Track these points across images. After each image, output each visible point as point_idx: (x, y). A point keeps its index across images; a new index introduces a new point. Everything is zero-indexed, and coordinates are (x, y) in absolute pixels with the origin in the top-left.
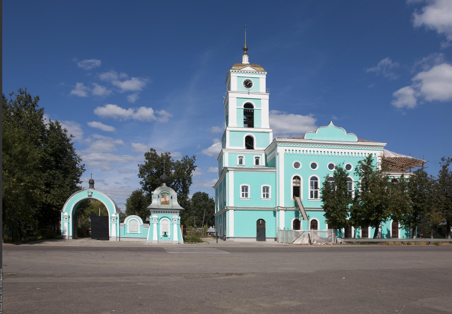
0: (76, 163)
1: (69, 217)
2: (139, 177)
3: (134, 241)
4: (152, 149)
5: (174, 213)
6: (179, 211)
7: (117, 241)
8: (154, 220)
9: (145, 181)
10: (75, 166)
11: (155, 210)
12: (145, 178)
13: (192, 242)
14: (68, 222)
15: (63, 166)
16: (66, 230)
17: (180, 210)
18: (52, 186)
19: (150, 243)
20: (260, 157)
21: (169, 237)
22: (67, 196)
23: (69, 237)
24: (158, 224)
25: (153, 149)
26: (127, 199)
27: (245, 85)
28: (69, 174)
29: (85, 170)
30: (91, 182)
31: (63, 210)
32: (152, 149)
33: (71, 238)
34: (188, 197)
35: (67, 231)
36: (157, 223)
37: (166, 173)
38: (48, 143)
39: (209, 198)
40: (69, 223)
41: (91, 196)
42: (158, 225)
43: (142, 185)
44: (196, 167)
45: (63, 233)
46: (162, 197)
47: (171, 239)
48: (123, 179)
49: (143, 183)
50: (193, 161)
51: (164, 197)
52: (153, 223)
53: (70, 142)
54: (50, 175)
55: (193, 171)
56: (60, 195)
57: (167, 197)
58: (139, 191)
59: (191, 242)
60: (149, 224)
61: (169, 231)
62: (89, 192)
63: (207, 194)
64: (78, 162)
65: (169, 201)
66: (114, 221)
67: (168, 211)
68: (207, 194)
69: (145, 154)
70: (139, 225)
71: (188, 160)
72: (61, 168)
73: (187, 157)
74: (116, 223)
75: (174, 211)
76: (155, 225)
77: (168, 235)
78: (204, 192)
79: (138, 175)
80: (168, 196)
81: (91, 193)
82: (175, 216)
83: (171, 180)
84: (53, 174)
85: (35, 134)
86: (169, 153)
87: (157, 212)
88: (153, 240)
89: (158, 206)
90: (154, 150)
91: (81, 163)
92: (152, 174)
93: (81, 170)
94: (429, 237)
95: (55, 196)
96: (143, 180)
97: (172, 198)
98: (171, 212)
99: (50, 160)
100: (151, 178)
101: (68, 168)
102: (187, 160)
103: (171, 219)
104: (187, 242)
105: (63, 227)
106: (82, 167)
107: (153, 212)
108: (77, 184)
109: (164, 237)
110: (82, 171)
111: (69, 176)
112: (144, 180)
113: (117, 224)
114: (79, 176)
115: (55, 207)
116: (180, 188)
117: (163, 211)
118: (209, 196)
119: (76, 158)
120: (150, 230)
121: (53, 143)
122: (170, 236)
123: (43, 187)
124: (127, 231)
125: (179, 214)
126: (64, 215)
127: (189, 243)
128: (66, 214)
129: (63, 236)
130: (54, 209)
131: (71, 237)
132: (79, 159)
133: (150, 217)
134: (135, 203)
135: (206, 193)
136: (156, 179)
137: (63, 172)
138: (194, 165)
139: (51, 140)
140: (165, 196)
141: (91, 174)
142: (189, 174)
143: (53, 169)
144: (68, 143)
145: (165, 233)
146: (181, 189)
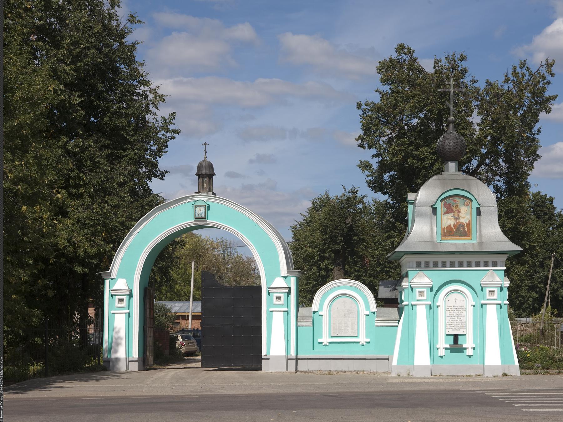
0: (148, 111)
1: (131, 296)
2: (359, 145)
3: (344, 369)
4: (401, 49)
5: (486, 264)
6: (504, 258)
7: (289, 370)
8: (417, 293)
10: (144, 118)
11: (423, 259)
12: (379, 149)
13: (546, 368)
14: (128, 311)
15: (106, 123)
16: (119, 341)
18: (74, 191)
19: (403, 378)
21: (469, 352)
22: (122, 223)
23: (128, 362)
24: (430, 308)
25: (404, 48)
26: (294, 228)
28: (125, 150)
29: (177, 132)
30: (204, 171)
31: (111, 272)
32: (401, 49)
33: (134, 367)
35: (123, 342)
36: (426, 305)
37: (457, 126)
38: (63, 47)
39: (556, 212)
40: (129, 315)
41: (204, 219)
44: (552, 102)
45: (110, 351)
46: (445, 210)
47: (476, 362)
48: (251, 161)
50: (544, 78)
51: (454, 210)
52: (413, 303)
53: (129, 40)
54: (68, 153)
55: (542, 115)
56: (99, 220)
57: (463, 209)
59: (543, 371)
60: (395, 309)
61: (469, 331)
62: (197, 204)
63: (548, 197)
64: (151, 108)
65: (468, 225)
66: (279, 302)
67: (465, 259)
68: (548, 197)
69: (378, 65)
70: (363, 311)
71: (526, 78)
72: (100, 129)
73: (522, 65)
74: (286, 309)
75: (486, 260)
76: (421, 312)
77: (464, 346)
78: (539, 193)
79: (357, 140)
80: (467, 205)
81: (203, 209)
84: (77, 150)
85: (23, 19)
86: (463, 58)
87: (427, 265)
88: (396, 365)
89: (433, 243)
90: (409, 49)
91: (163, 112)
92: (402, 134)
93: (163, 132)
95: (84, 224)
96: (373, 156)
97: (479, 213)
98: (478, 264)
99: (70, 103)
100: (402, 148)
101: (123, 128)
102: (523, 76)
103: (478, 289)
105: (112, 328)
106: (166, 123)
107: (415, 265)
108: (148, 182)
110: (168, 135)
111: (125, 154)
112: (378, 155)
113: (287, 312)
114: (159, 153)
115: (83, 264)
116: (498, 178)
117: (448, 259)
118: (555, 203)
119: (147, 93)
121: (76, 48)
122: (474, 349)
123: (59, 195)
124: (321, 336)
125: (505, 268)
126: (114, 289)
128: (121, 284)
129: (108, 361)
130: (79, 269)
131: (137, 363)
132: (155, 98)
133: (405, 284)
134: (333, 239)
135: (546, 195)
137: (107, 142)
138: (547, 94)
139: (70, 37)
140: (457, 206)
141: (205, 144)
142: (530, 127)
143: (77, 135)
144: (121, 44)
145: (456, 337)
146: (499, 181)
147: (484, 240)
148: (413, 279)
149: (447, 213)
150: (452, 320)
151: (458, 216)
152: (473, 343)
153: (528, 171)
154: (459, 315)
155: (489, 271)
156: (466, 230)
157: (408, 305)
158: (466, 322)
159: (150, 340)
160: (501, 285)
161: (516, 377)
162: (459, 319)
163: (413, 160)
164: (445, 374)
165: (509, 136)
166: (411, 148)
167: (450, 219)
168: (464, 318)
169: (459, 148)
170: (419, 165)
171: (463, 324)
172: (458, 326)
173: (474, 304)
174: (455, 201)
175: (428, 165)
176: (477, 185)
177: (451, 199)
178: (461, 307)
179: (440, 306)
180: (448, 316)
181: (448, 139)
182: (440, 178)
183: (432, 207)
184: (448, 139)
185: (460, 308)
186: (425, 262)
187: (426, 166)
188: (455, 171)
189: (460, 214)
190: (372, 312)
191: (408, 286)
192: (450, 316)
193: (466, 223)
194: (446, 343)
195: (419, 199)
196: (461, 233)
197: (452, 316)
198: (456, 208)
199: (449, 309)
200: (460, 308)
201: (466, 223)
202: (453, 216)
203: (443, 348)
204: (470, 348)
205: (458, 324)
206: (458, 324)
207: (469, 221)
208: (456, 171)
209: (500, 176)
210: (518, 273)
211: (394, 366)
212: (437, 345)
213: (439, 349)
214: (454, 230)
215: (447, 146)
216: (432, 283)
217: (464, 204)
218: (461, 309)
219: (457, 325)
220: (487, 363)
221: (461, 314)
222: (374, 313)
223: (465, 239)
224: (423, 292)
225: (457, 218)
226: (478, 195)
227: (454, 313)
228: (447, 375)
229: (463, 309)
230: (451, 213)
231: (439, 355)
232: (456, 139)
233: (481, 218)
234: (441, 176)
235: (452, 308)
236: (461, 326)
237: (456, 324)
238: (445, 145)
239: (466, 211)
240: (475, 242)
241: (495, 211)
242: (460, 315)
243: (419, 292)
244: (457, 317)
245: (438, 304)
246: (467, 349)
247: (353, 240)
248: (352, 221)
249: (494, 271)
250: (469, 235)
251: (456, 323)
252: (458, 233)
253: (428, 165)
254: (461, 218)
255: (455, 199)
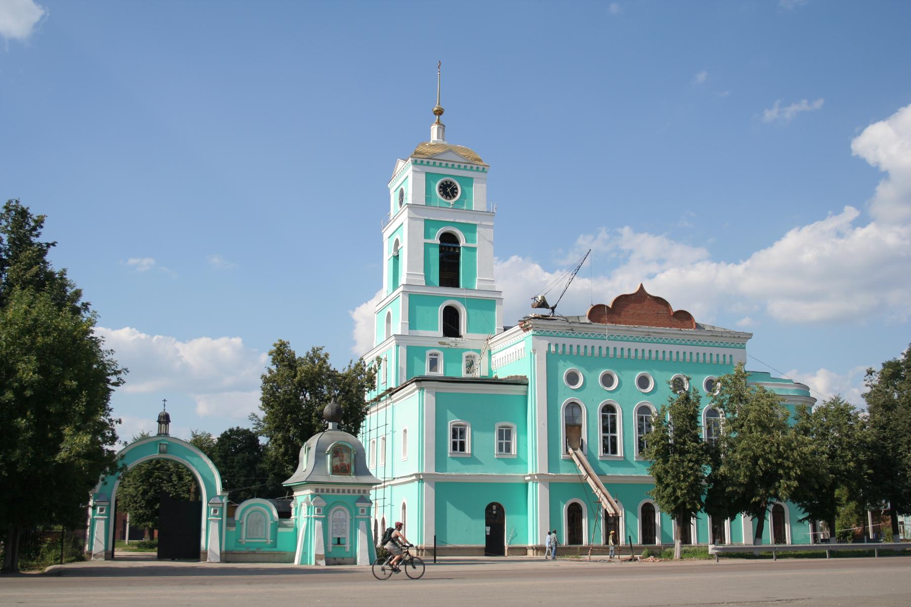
20: (439, 354)
27: (442, 192)
51: (340, 455)
57: (346, 455)
61: (347, 536)
94: (716, 533)
140: (342, 453)
141: (165, 400)
145: (339, 539)
159: (653, 527)
225: (341, 461)
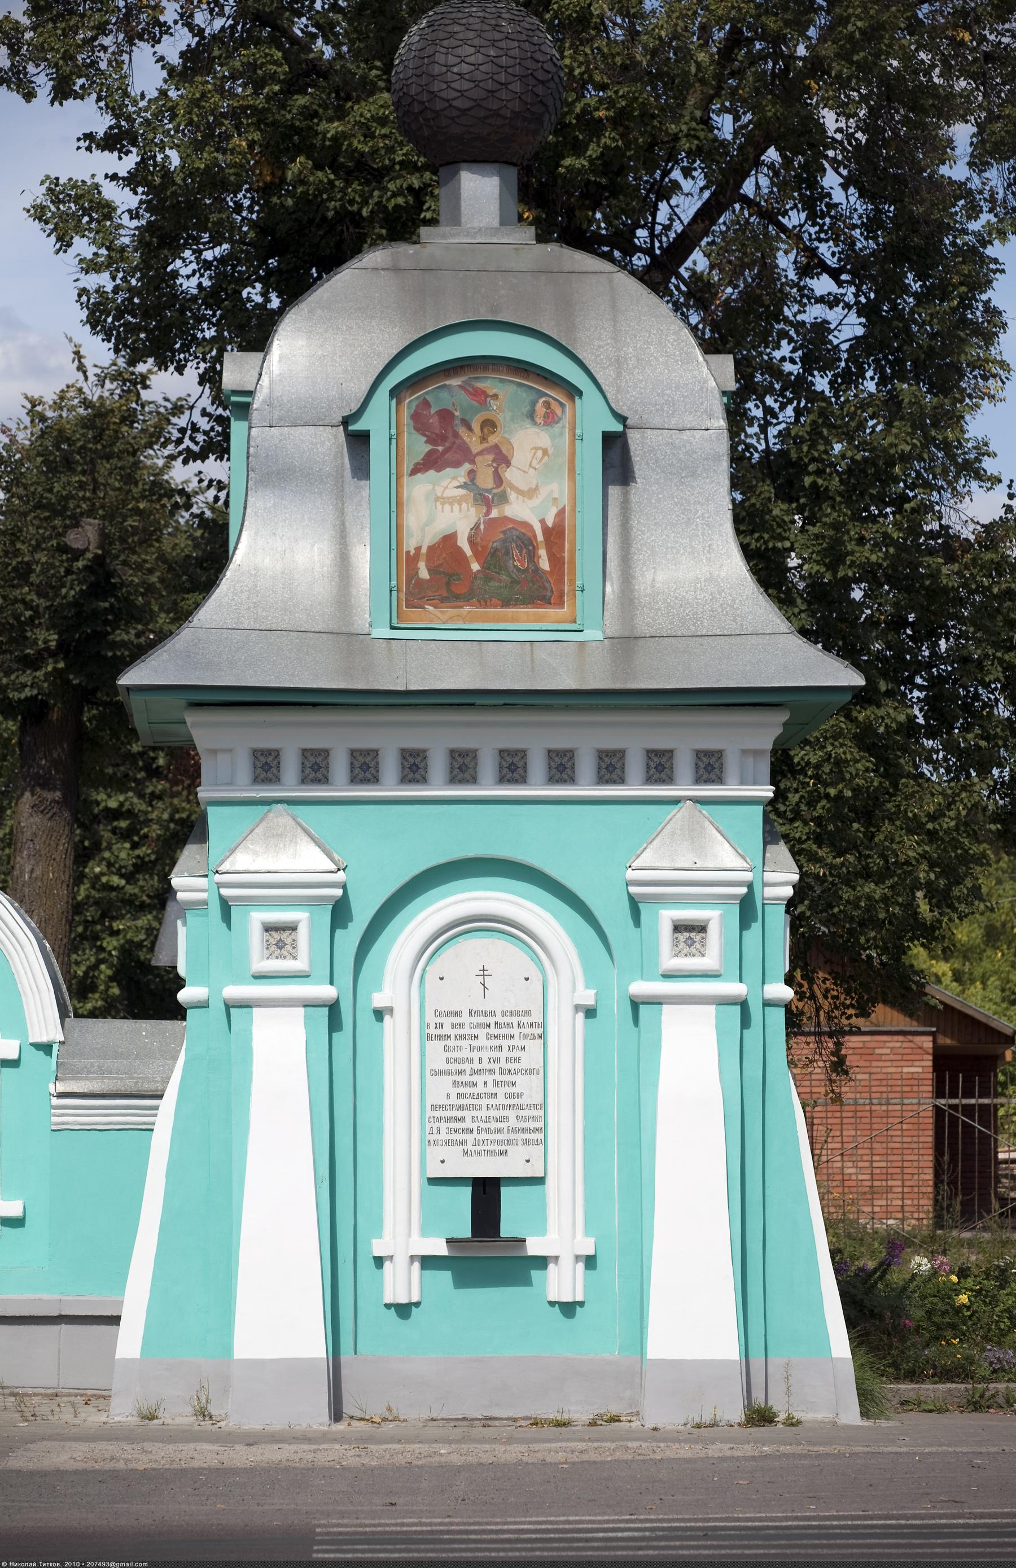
8: (256, 936)
9: (131, 161)
17: (784, 716)
24: (335, 1023)
34: (983, 450)
36: (309, 1004)
42: (343, 1039)
43: (83, 247)
46: (419, 447)
49: (107, 209)
51: (474, 443)
52: (233, 991)
58: (93, 393)
77: (534, 1247)
80: (550, 419)
82: (694, 836)
83: (620, 119)
88: (240, 1352)
104: (931, 1390)
109: (462, 1281)
120: (179, 1132)
122: (590, 1262)
127: (976, 1405)
136: (341, 114)
140: (489, 425)
146: (831, 301)
147: (644, 623)
148: (233, 851)
149: (430, 463)
150: (460, 1096)
151: (499, 480)
152: (587, 1233)
153: (985, 244)
154: (503, 1064)
155: (674, 809)
156: (545, 564)
157: (203, 1005)
158: (544, 1106)
160: (744, 890)
161: (834, 1430)
162: (501, 1091)
163: (320, 174)
164: (415, 1413)
165: (852, 35)
166: (301, 100)
167: (452, 501)
168: (536, 1081)
169: (516, 87)
170: (352, 202)
171: (525, 1119)
172: (499, 1131)
173: (590, 1002)
174: (481, 397)
175: (400, 200)
176: (614, 307)
177: (455, 382)
178: (515, 1020)
179: (390, 1010)
180: (442, 1073)
181: (452, 35)
182: (403, 264)
183: (346, 429)
184: (452, 35)
185: (509, 1025)
186: (305, 753)
187: (391, 205)
188: (496, 223)
189: (510, 475)
190: (38, 1046)
191: (203, 896)
192: (448, 1073)
193: (543, 522)
194: (425, 1231)
195: (271, 382)
196: (514, 582)
197: (459, 1072)
198: (483, 439)
199: (447, 1030)
200: (509, 1025)
201: (543, 522)
202: (464, 486)
203: (412, 1258)
204: (567, 1261)
205: (499, 1120)
206: (499, 1120)
207: (561, 513)
208: (503, 223)
209: (834, 274)
210: (930, 826)
211: (126, 1361)
212: (375, 1242)
213: (387, 1264)
214: (475, 567)
215: (449, 77)
216: (341, 876)
217: (531, 415)
218: (516, 1031)
219: (493, 1125)
220: (658, 1348)
221: (517, 1060)
222: (46, 1048)
223: (539, 619)
224: (293, 928)
226: (619, 363)
227: (476, 1055)
228: (425, 1415)
229: (527, 1031)
230: (457, 464)
231: (388, 1300)
232: (497, 36)
233: (634, 498)
234: (411, 249)
235: (461, 1025)
236: (514, 1130)
237: (488, 1120)
238: (436, 71)
239: (545, 452)
240: (593, 634)
241: (717, 458)
242: (509, 1066)
243: (269, 928)
244: (490, 1079)
245: (379, 1000)
246: (551, 1266)
247: (114, 645)
248: (105, 539)
249: (706, 810)
250: (561, 596)
251: (484, 1113)
252: (494, 584)
253: (400, 200)
254: (513, 496)
255: (480, 385)
